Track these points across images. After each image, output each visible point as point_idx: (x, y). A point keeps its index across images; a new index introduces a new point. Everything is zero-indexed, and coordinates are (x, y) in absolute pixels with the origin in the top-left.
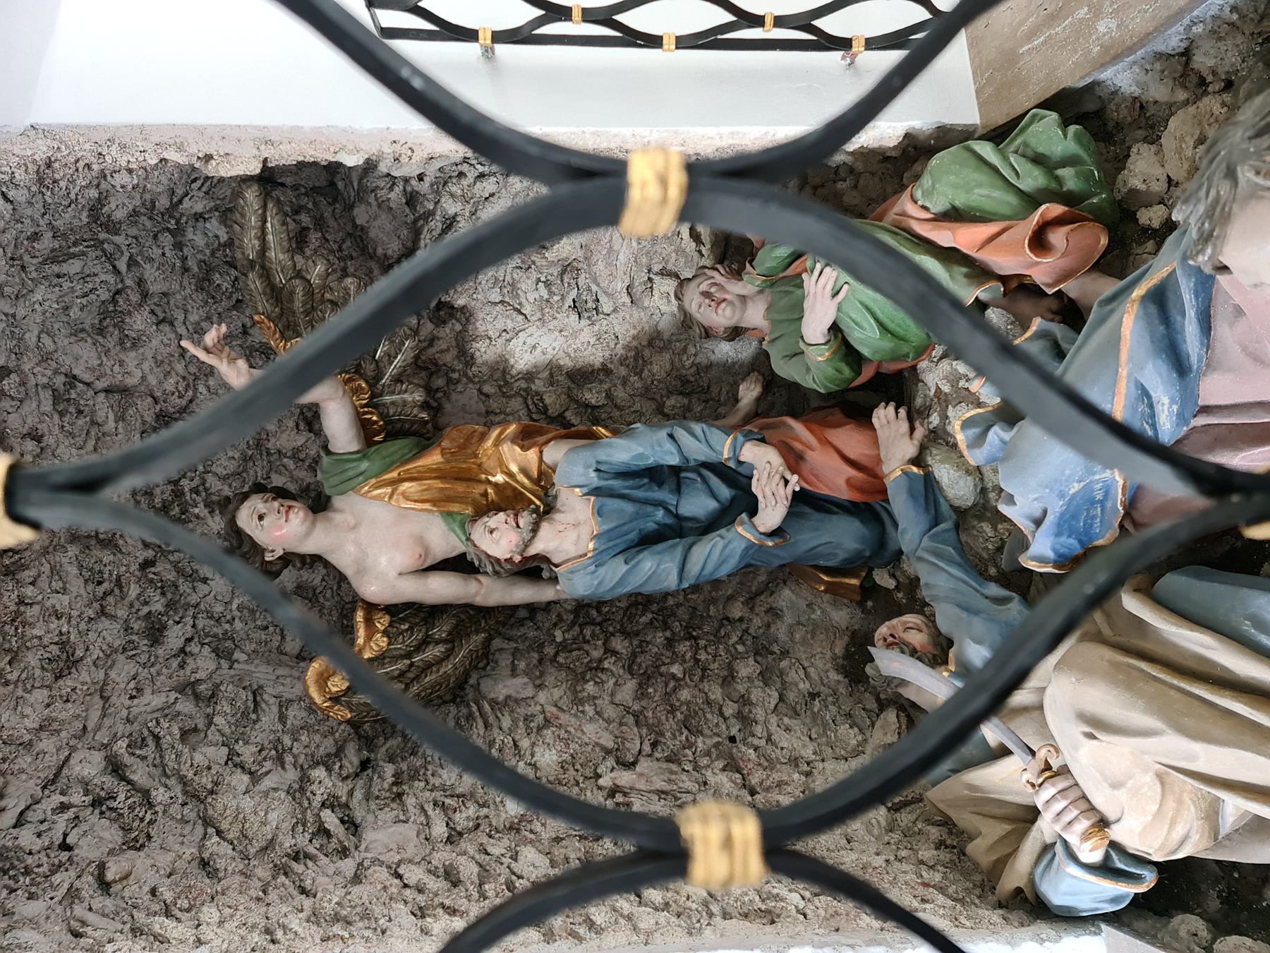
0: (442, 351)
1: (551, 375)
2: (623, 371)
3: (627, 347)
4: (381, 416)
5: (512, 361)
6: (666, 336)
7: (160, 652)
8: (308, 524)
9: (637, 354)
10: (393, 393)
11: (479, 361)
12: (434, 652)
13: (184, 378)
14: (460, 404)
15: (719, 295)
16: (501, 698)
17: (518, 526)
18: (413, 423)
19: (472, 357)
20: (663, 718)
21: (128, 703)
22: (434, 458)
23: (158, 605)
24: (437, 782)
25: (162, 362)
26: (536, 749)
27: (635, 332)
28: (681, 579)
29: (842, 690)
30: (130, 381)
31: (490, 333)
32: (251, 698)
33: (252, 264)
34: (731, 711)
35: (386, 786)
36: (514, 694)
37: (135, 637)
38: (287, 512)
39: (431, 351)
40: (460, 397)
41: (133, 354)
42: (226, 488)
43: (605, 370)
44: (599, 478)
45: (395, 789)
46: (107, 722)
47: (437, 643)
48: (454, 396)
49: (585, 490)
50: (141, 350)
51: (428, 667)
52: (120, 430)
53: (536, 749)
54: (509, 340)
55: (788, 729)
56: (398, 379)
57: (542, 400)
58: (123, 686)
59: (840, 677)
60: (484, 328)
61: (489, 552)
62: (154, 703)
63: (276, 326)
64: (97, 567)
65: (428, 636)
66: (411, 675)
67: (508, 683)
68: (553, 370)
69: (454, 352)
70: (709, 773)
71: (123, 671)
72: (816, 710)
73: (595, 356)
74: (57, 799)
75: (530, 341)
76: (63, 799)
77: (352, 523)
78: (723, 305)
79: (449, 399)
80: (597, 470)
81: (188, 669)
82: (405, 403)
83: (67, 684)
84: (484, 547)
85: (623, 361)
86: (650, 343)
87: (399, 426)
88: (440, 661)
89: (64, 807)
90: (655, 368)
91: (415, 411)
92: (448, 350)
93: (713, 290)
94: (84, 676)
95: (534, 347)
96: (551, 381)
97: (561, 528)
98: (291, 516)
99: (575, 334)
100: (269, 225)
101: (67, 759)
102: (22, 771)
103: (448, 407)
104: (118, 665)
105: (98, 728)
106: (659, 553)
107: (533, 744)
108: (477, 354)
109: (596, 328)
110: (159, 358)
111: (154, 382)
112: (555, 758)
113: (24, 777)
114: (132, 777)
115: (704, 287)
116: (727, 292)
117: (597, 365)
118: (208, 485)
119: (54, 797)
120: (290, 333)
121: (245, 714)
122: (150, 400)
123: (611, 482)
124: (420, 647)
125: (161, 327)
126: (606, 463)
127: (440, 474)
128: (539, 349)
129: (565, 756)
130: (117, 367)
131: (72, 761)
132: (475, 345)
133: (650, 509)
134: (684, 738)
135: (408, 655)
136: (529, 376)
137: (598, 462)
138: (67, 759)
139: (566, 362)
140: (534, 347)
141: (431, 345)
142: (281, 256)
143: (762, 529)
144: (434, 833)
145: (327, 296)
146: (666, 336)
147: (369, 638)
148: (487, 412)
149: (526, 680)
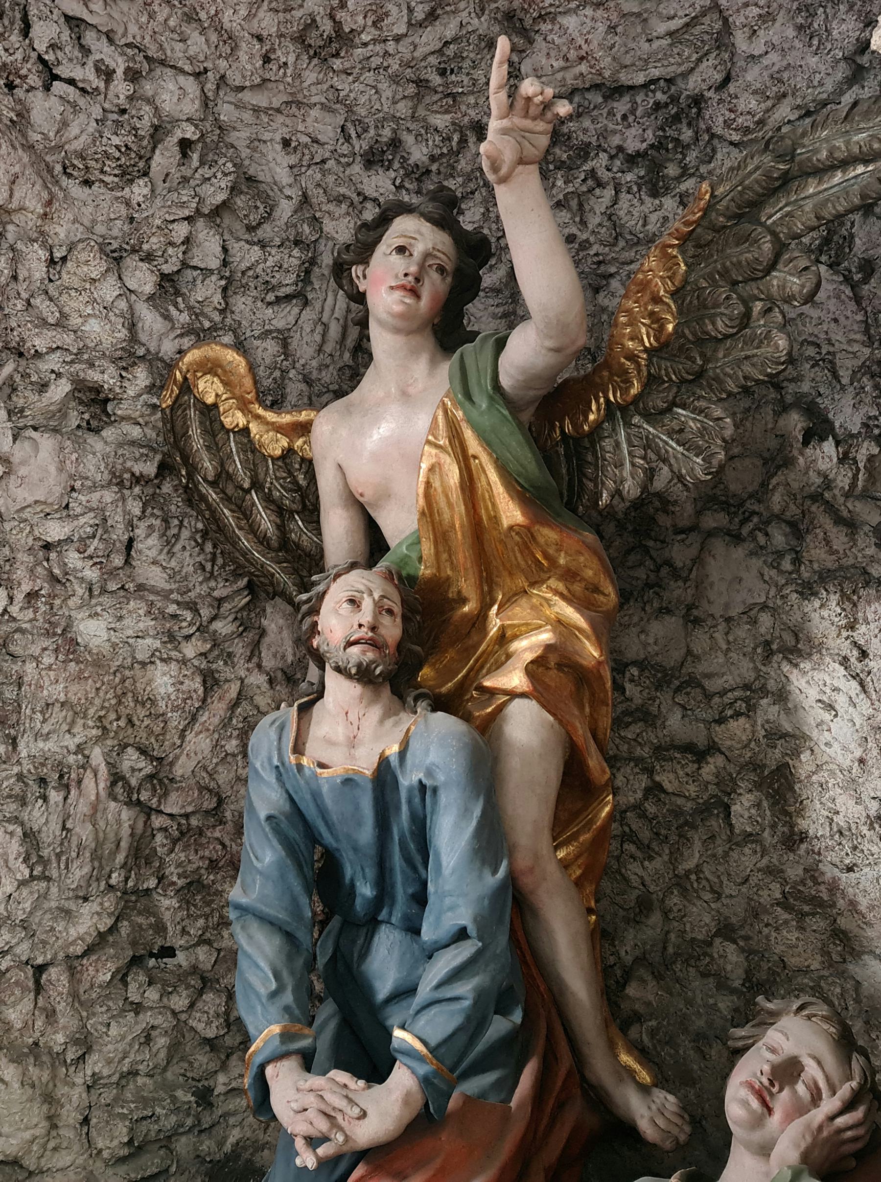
0: (828, 542)
1: (784, 736)
2: (794, 873)
3: (834, 887)
4: (598, 426)
5: (806, 665)
6: (851, 967)
7: (357, 168)
8: (399, 323)
9: (821, 903)
10: (630, 444)
11: (808, 607)
12: (266, 522)
13: (761, 122)
14: (744, 575)
15: (782, 1100)
16: (265, 622)
17: (350, 644)
18: (595, 480)
19: (815, 594)
20: (207, 853)
21: (278, 138)
22: (511, 513)
23: (418, 154)
24: (140, 532)
25: (780, 81)
26: (173, 665)
27: (863, 908)
28: (238, 907)
29: (207, 1145)
30: (740, 40)
31: (863, 629)
32: (288, 290)
33: (789, 156)
34: (202, 957)
35: (129, 464)
36: (266, 640)
37: (372, 132)
38: (403, 287)
39: (826, 521)
40: (754, 572)
41: (791, 32)
42: (597, 220)
43: (794, 839)
44: (410, 789)
45: (127, 476)
46: (247, 116)
47: (278, 527)
48: (756, 563)
49: (394, 761)
50: (797, 44)
51: (244, 513)
52: (656, 44)
53: (173, 665)
54: (844, 661)
55: (148, 1039)
56: (648, 444)
57: (737, 715)
58: (301, 127)
59: (228, 1147)
60: (871, 616)
61: (327, 597)
62: (278, 170)
63: (698, 223)
64: (466, 64)
65: (292, 512)
66: (230, 490)
67: (285, 633)
68: (794, 740)
69: (830, 562)
70: (96, 907)
71: (324, 126)
72: (179, 1093)
73: (814, 822)
74: (120, 65)
75: (841, 702)
76: (120, 72)
77: (411, 390)
78: (755, 1104)
79: (752, 554)
80: (422, 787)
81: (331, 207)
82: (620, 465)
83: (287, 53)
84: (334, 587)
85: (812, 873)
86: (841, 936)
87: (590, 458)
88: (253, 530)
89: (108, 75)
90: (793, 936)
91: (610, 484)
92: (832, 552)
93: (801, 1088)
94: (310, 76)
95: (830, 707)
96: (775, 735)
97: (352, 717)
98: (398, 294)
99: (852, 785)
100: (860, 169)
101: (182, 71)
102: (152, 16)
103: (739, 553)
104: (328, 118)
105: (239, 106)
106: (282, 876)
107: (184, 662)
108: (817, 603)
109: (865, 830)
110: (785, 75)
111: (749, 77)
112: (162, 691)
113: (144, 19)
114: (157, 152)
115: (811, 1069)
116: (789, 1118)
117: (803, 824)
118: (598, 191)
119: (120, 60)
120: (691, 251)
121: (269, 287)
122: (718, 77)
123: (404, 808)
124: (268, 500)
125: (842, 64)
126: (435, 803)
127: (479, 528)
128: (827, 716)
129: (162, 704)
130: (756, 11)
131: (181, 79)
132: (834, 599)
133: (371, 873)
134: (175, 879)
135: (256, 485)
136: (782, 696)
137: (435, 790)
138: (182, 71)
139: (805, 764)
140: (830, 707)
141: (839, 520)
142: (809, 206)
143: (269, 1071)
144: (51, 523)
145: (758, 306)
146: (851, 967)
147: (279, 429)
148: (728, 620)
149: (290, 658)
